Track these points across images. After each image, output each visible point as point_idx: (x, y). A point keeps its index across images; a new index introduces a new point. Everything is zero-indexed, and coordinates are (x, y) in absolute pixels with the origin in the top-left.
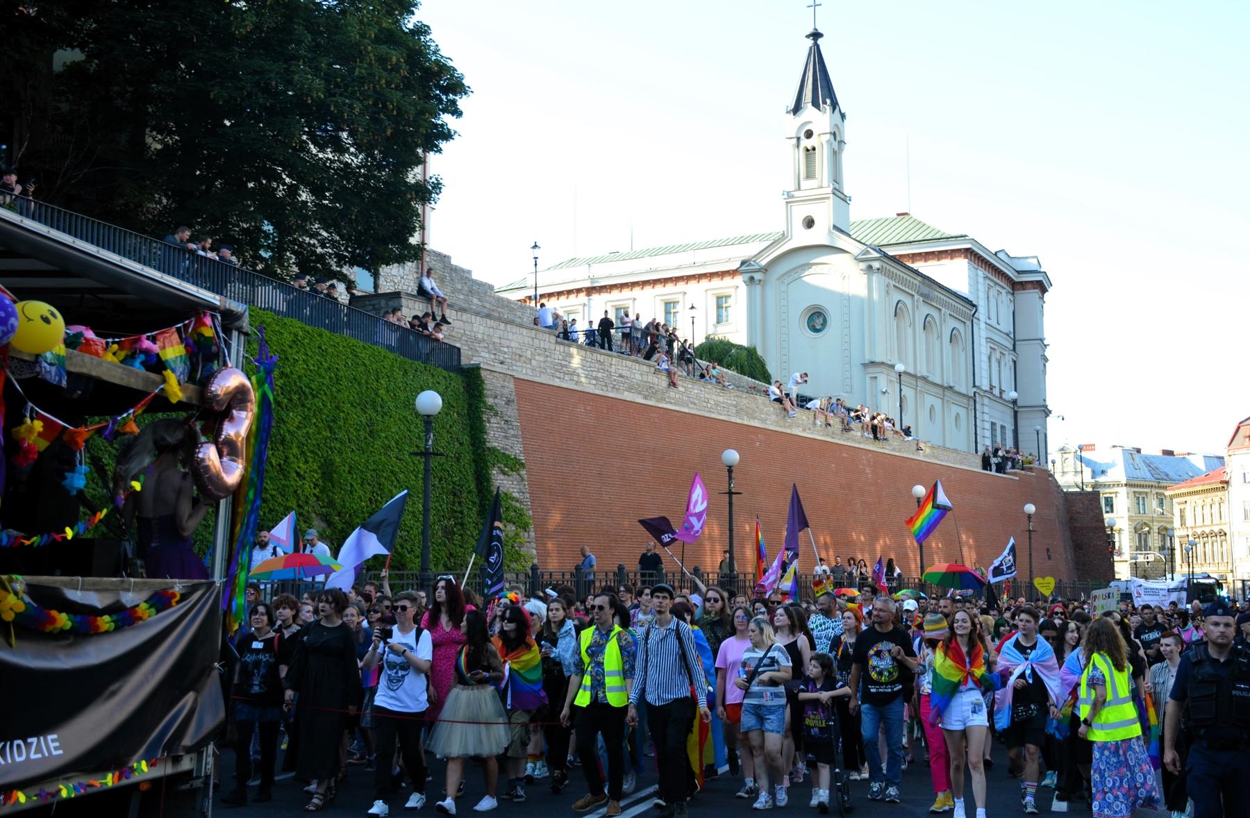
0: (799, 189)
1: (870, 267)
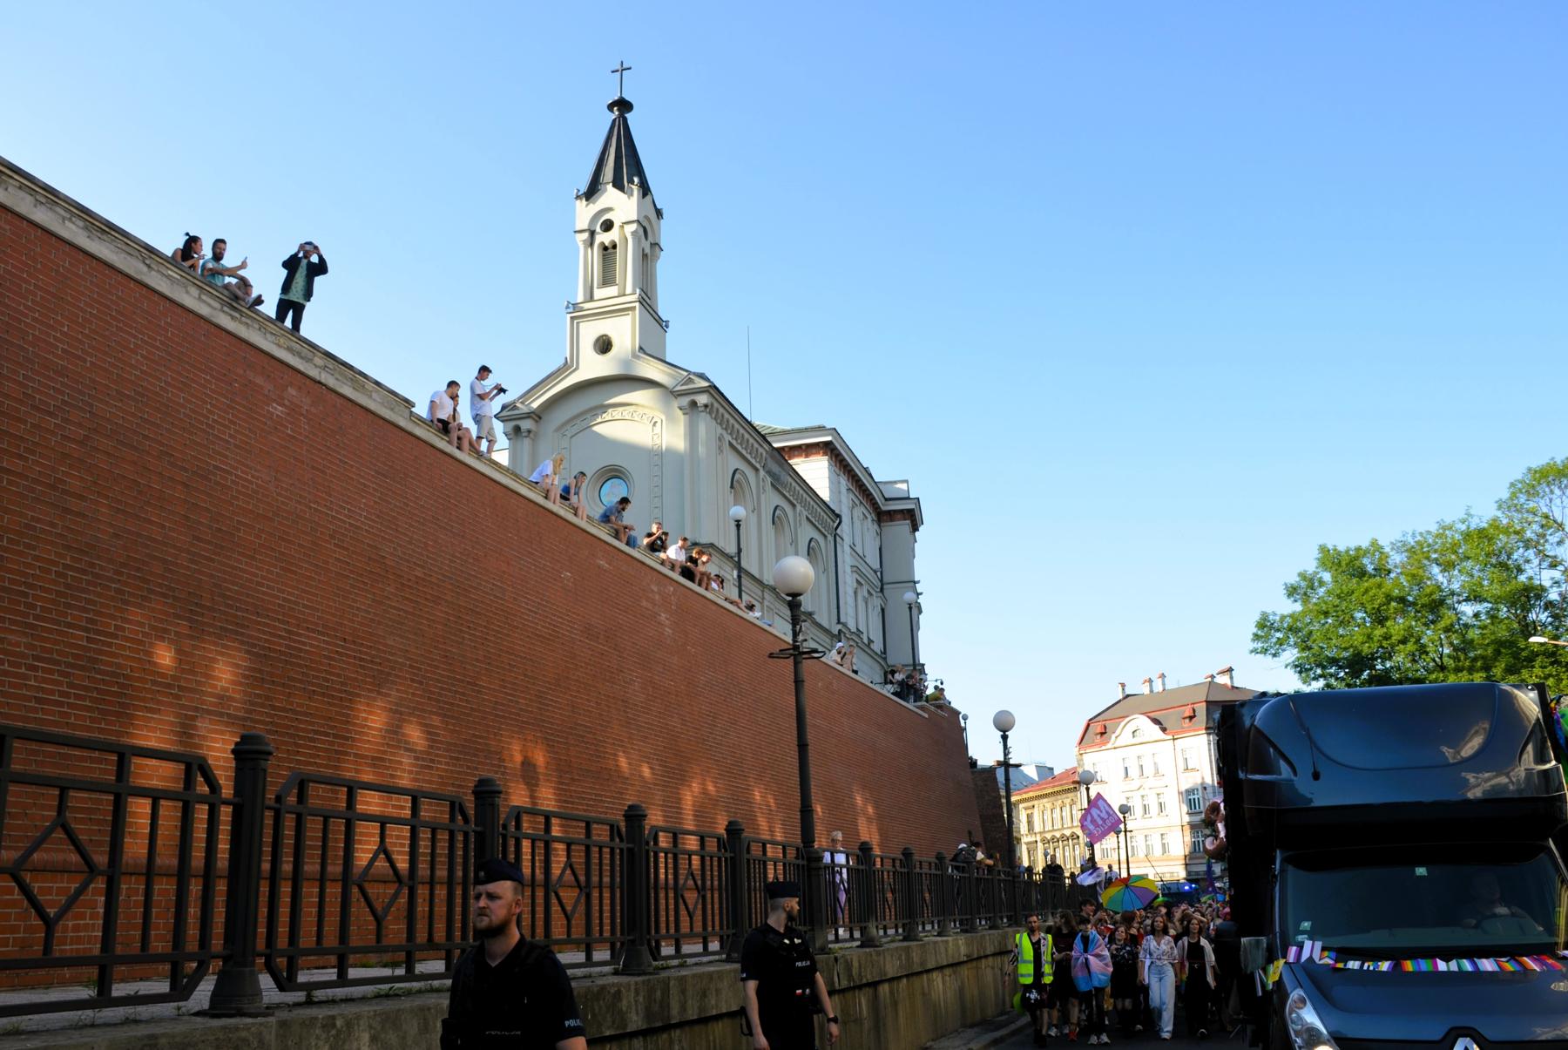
0: (591, 299)
1: (694, 404)
